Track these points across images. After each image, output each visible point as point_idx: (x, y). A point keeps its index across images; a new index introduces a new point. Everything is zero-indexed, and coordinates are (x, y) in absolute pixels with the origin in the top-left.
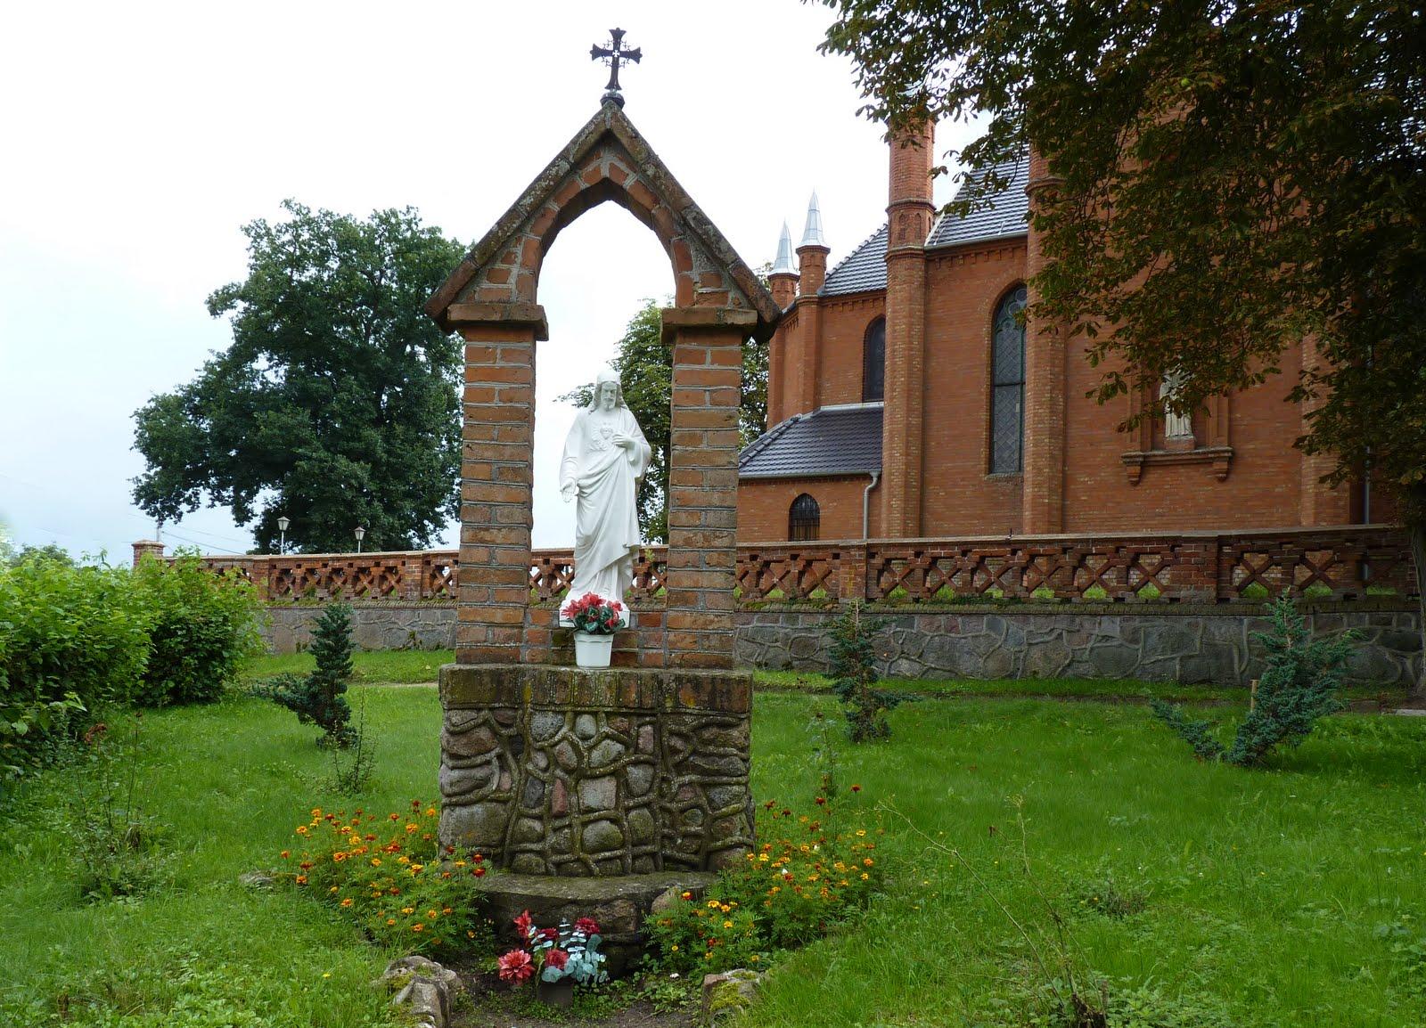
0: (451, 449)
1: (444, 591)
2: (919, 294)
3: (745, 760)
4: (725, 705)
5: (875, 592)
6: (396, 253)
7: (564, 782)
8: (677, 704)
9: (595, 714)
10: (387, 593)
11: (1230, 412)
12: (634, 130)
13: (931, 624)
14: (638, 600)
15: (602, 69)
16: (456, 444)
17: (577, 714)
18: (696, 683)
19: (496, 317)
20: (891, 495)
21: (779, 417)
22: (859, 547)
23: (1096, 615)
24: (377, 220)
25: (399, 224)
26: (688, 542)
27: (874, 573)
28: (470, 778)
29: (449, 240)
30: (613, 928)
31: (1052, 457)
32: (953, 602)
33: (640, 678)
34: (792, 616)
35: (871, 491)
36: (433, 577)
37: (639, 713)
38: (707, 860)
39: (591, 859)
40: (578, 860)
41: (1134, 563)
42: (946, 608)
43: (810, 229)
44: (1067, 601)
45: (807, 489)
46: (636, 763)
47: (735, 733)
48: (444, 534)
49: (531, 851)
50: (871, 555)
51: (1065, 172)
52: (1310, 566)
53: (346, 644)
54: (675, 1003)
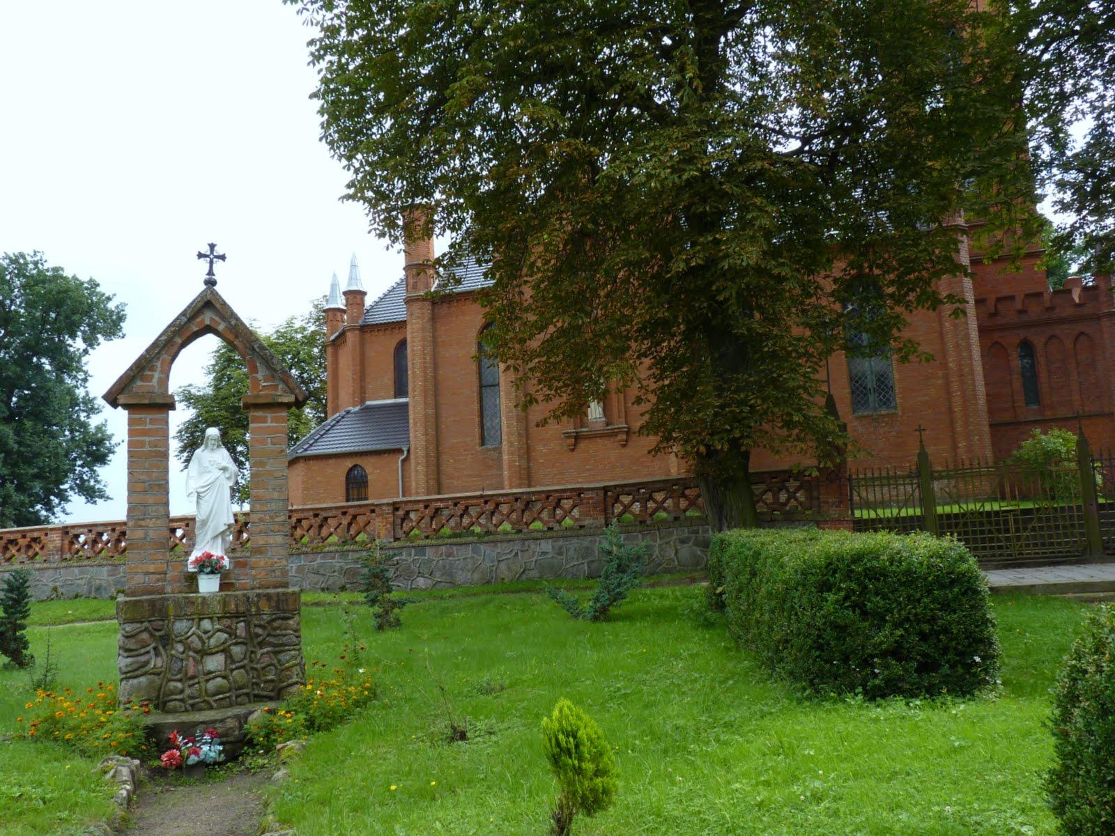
0: (73, 438)
1: (81, 553)
2: (428, 326)
3: (298, 637)
4: (285, 607)
5: (400, 534)
6: (23, 287)
7: (194, 659)
8: (258, 608)
9: (211, 618)
10: (32, 558)
11: (625, 403)
12: (223, 300)
13: (437, 552)
14: (233, 550)
15: (204, 265)
16: (77, 434)
17: (201, 619)
18: (269, 597)
19: (147, 402)
20: (417, 464)
21: (336, 410)
22: (388, 504)
23: (537, 539)
24: (7, 261)
25: (26, 264)
26: (261, 520)
27: (399, 521)
28: (137, 662)
29: (70, 276)
30: (226, 735)
31: (519, 434)
32: (450, 537)
33: (236, 596)
34: (344, 554)
35: (403, 461)
36: (72, 543)
37: (237, 616)
38: (278, 694)
39: (211, 700)
40: (204, 701)
41: (558, 504)
42: (447, 541)
43: (352, 278)
44: (520, 531)
45: (358, 461)
46: (236, 644)
47: (291, 622)
48: (68, 506)
49: (175, 700)
50: (397, 509)
51: (493, 277)
52: (655, 501)
53: (26, 596)
54: (263, 767)
